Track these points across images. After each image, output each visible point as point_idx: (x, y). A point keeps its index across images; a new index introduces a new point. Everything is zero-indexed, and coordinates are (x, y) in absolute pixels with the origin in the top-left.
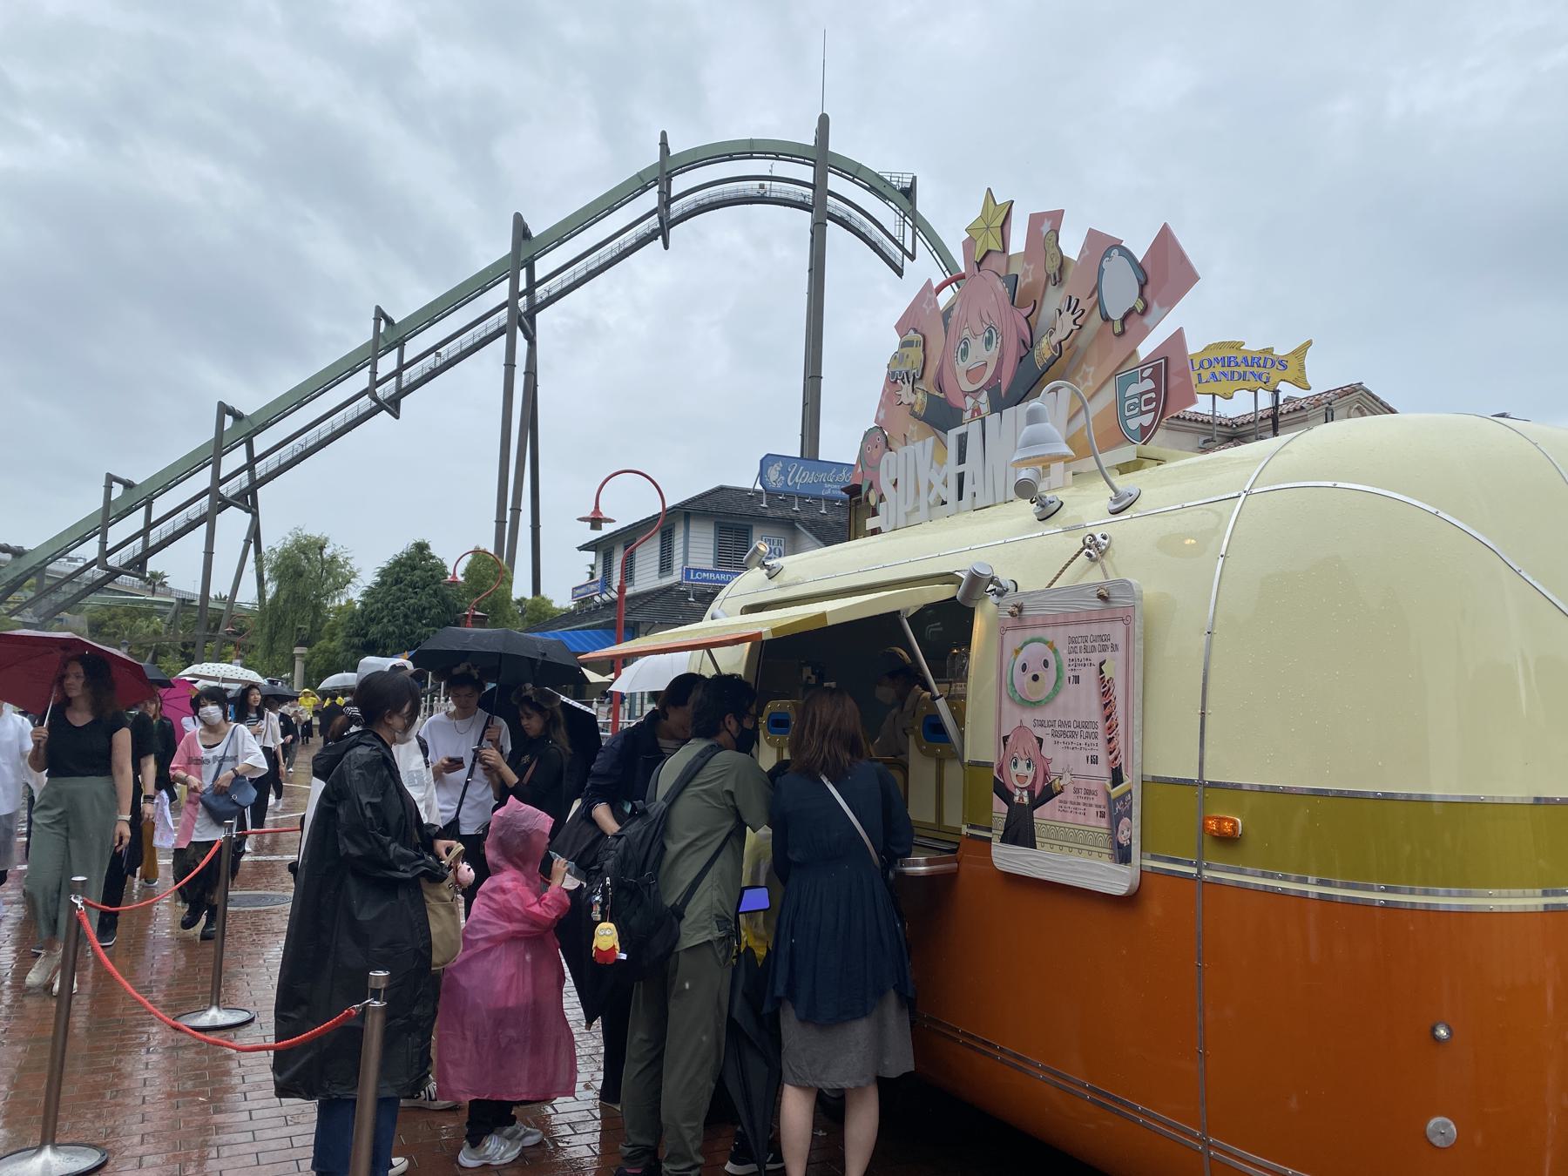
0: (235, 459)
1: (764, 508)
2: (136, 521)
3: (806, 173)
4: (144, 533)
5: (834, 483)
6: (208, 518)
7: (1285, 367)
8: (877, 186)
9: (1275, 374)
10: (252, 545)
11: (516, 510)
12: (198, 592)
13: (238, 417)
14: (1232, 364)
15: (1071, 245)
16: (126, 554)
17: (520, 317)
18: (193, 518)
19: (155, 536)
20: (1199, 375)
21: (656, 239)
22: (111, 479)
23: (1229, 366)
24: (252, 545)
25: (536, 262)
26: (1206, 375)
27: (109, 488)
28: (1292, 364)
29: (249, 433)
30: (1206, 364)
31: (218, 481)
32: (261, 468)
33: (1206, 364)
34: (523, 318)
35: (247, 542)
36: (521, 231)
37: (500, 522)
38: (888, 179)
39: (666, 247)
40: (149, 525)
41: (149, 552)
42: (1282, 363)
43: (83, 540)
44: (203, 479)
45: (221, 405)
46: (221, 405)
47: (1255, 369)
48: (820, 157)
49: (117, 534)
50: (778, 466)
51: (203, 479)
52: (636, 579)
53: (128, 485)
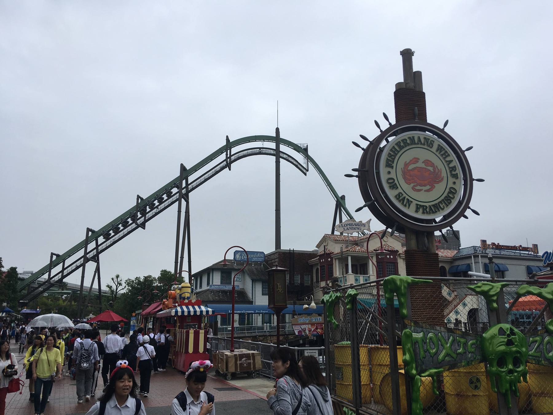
0: (92, 246)
1: (235, 266)
2: (59, 268)
3: (273, 145)
4: (62, 272)
5: (256, 257)
6: (83, 265)
7: (365, 226)
8: (296, 148)
9: (362, 228)
10: (97, 273)
11: (182, 257)
12: (80, 284)
13: (93, 231)
14: (352, 225)
15: (16, 377)
16: (56, 278)
17: (183, 195)
18: (78, 265)
19: (65, 272)
20: (344, 228)
21: (227, 168)
22: (52, 254)
23: (351, 226)
24: (97, 273)
25: (189, 177)
26: (345, 228)
27: (52, 257)
28: (367, 226)
29: (97, 237)
30: (346, 226)
31: (86, 253)
32: (100, 248)
33: (346, 226)
34: (184, 196)
35: (95, 272)
36: (183, 168)
37: (296, 166)
38: (300, 146)
39: (230, 170)
40: (64, 269)
41: (64, 277)
42: (364, 225)
43: (43, 274)
44: (81, 253)
45: (88, 229)
46: (88, 229)
47: (358, 227)
48: (277, 139)
49: (54, 271)
50: (239, 254)
51: (81, 253)
52: (202, 286)
53: (58, 256)
